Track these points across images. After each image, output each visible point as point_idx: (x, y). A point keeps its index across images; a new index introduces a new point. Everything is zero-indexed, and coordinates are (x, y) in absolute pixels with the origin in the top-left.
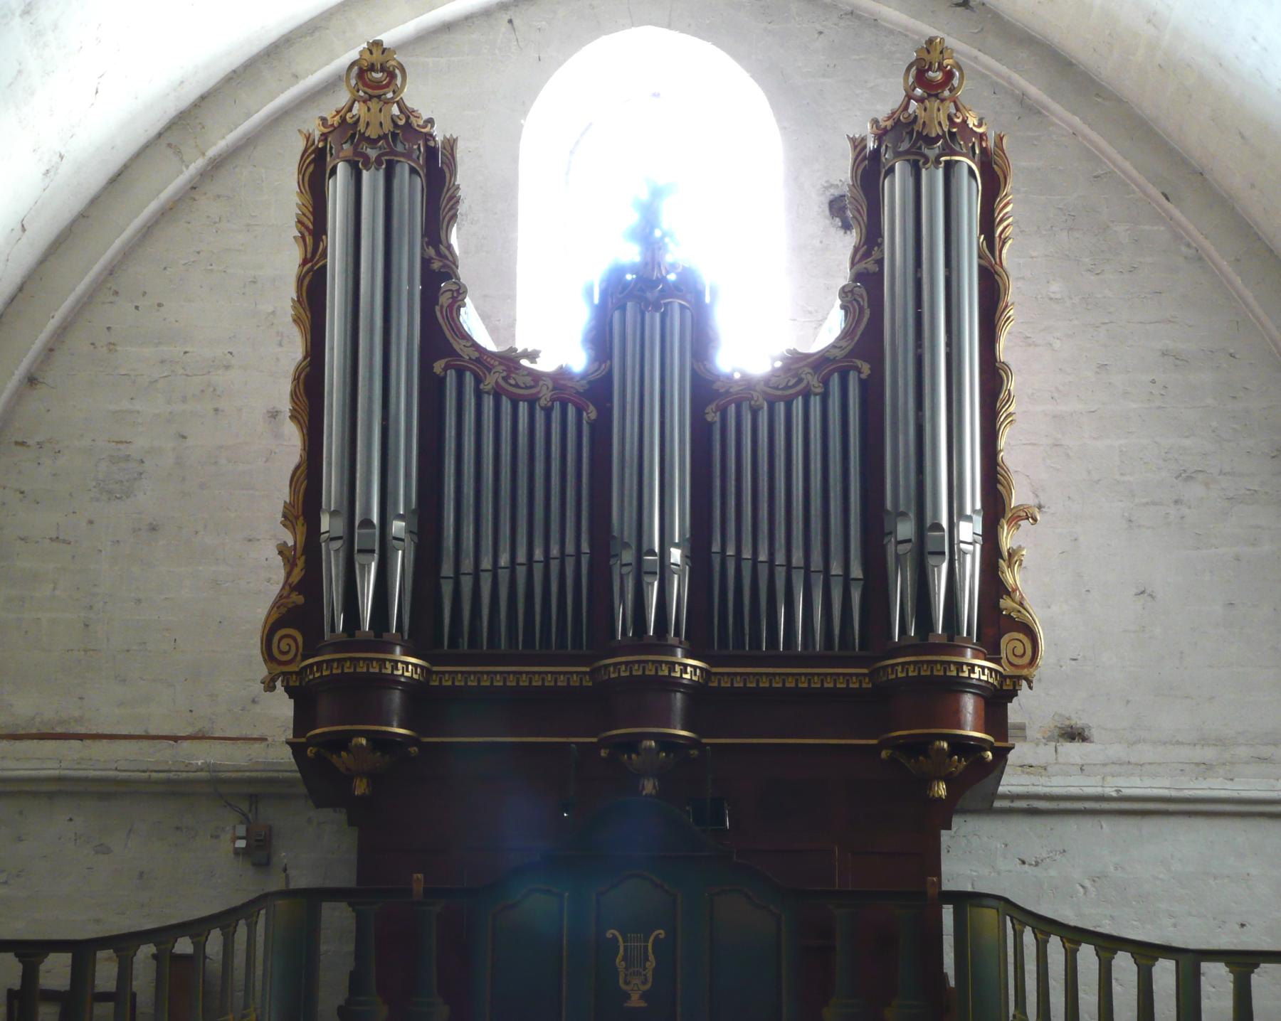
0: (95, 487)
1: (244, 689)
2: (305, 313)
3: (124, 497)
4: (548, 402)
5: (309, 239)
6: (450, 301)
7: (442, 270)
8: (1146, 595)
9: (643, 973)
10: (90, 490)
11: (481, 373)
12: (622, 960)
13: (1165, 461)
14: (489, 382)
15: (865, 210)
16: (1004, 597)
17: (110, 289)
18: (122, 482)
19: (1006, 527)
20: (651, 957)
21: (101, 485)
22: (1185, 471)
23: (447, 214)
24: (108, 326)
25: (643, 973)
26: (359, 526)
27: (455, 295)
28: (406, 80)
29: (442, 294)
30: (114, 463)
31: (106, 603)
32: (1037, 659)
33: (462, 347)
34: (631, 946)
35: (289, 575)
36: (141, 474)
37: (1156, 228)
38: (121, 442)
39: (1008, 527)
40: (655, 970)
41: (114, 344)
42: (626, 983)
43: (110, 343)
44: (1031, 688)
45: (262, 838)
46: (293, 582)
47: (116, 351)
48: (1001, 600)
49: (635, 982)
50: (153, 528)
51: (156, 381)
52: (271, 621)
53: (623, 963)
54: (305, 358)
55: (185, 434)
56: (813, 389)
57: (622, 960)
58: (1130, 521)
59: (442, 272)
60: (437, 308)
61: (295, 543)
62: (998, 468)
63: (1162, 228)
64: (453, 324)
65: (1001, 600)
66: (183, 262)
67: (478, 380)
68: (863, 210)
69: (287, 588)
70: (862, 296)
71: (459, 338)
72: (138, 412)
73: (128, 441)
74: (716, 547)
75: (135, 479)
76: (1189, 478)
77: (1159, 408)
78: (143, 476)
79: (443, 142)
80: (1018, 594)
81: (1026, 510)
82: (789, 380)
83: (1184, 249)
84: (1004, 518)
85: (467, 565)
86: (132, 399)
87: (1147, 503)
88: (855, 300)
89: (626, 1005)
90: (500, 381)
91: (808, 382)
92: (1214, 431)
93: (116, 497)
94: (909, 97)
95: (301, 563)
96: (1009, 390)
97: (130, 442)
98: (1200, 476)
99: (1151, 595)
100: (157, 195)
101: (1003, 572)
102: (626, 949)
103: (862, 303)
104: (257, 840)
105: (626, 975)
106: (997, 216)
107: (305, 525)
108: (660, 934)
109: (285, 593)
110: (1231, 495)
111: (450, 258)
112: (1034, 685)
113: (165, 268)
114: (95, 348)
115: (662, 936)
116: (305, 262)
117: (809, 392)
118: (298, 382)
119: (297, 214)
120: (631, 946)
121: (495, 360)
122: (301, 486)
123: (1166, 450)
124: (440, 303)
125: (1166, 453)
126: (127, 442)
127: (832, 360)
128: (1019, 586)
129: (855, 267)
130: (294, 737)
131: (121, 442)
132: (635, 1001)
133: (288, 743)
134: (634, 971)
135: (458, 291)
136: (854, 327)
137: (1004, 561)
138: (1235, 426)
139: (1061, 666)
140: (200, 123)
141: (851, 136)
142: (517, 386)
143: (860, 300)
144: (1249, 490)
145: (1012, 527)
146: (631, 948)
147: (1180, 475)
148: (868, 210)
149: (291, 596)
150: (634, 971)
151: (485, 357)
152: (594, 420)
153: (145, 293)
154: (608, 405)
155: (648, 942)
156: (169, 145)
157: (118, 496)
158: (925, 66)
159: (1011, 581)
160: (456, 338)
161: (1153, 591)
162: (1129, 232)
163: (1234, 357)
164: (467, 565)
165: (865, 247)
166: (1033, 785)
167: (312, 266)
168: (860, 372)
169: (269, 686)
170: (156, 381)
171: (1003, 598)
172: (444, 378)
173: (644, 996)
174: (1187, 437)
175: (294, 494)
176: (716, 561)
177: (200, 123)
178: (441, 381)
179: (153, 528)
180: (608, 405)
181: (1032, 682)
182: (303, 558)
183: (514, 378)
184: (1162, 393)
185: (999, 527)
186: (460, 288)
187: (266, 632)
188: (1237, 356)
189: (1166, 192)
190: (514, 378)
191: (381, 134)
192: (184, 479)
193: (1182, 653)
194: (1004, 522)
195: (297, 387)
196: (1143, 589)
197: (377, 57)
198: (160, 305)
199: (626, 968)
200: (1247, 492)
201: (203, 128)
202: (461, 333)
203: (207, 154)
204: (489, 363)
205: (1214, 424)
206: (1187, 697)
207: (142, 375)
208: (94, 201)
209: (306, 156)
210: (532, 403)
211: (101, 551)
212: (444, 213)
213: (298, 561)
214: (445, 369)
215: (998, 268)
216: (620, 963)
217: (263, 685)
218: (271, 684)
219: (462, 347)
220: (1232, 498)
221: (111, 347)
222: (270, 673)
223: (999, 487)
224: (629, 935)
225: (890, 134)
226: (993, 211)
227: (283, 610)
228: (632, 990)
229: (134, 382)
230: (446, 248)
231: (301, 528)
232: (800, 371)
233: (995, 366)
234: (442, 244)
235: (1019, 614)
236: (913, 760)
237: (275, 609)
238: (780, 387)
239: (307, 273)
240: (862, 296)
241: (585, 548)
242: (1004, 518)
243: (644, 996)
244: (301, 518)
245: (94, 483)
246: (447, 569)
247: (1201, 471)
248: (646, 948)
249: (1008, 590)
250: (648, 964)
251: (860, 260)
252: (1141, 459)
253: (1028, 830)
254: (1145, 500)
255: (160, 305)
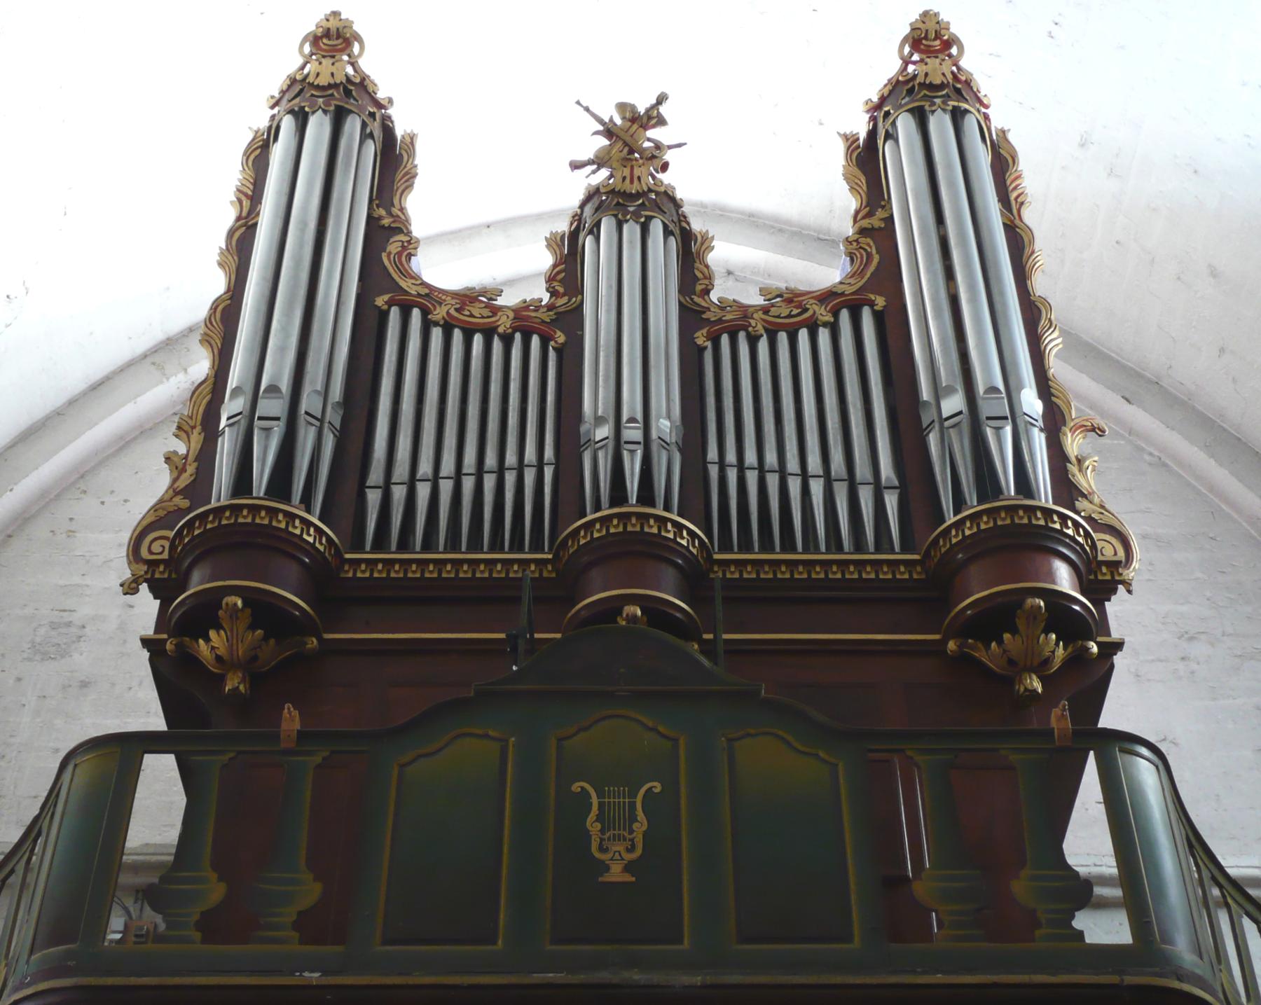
0: (29, 648)
1: (160, 835)
2: (233, 258)
3: (59, 657)
4: (508, 329)
5: (246, 203)
6: (400, 249)
7: (392, 225)
8: (1168, 742)
9: (628, 837)
10: (23, 651)
11: (430, 306)
12: (597, 821)
13: (1163, 624)
14: (439, 313)
15: (864, 182)
16: (1080, 499)
17: (79, 488)
18: (59, 645)
19: (1069, 435)
20: (640, 815)
21: (37, 648)
22: (1186, 633)
23: (401, 184)
24: (71, 517)
25: (628, 837)
26: (263, 392)
27: (406, 244)
28: (364, 46)
29: (391, 244)
30: (54, 629)
31: (20, 752)
32: (1132, 561)
33: (410, 285)
34: (609, 802)
35: (175, 481)
36: (81, 637)
37: (1116, 442)
38: (64, 611)
39: (1072, 435)
40: (645, 834)
41: (74, 532)
42: (602, 849)
43: (70, 531)
44: (1129, 592)
45: (144, 932)
46: (178, 487)
47: (75, 537)
48: (1076, 502)
49: (618, 848)
50: (84, 685)
51: (111, 560)
52: (145, 523)
53: (599, 826)
54: (225, 293)
55: (132, 604)
56: (820, 317)
57: (597, 821)
58: (1138, 676)
59: (393, 228)
60: (384, 256)
61: (188, 451)
62: (1050, 382)
63: (1122, 442)
64: (400, 267)
65: (1076, 502)
66: (155, 468)
67: (425, 312)
68: (861, 181)
69: (171, 492)
70: (868, 245)
71: (406, 277)
72: (88, 586)
73: (72, 609)
74: (712, 454)
75: (74, 642)
76: (1191, 639)
77: (1149, 580)
78: (82, 639)
79: (403, 137)
80: (1096, 497)
81: (1091, 421)
82: (792, 311)
83: (1147, 457)
84: (1065, 426)
85: (401, 470)
86: (83, 575)
87: (1153, 661)
88: (861, 248)
89: (600, 879)
90: (453, 312)
91: (815, 312)
92: (1208, 599)
93: (50, 657)
94: (906, 62)
95: (191, 469)
96: (1050, 319)
97: (74, 611)
98: (1203, 637)
99: (1172, 742)
100: (135, 398)
101: (1073, 476)
102: (601, 805)
103: (869, 250)
104: (136, 936)
105: (602, 840)
106: (1010, 185)
107: (203, 434)
108: (655, 787)
109: (167, 497)
110: (1239, 653)
111: (403, 217)
112: (1134, 587)
113: (137, 472)
114: (54, 534)
115: (657, 790)
116: (239, 219)
117: (816, 322)
118: (215, 312)
119: (237, 186)
120: (614, 802)
121: (447, 296)
122: (204, 398)
123: (1163, 616)
124: (388, 251)
125: (1163, 618)
126: (70, 611)
127: (840, 294)
128: (1094, 487)
129: (856, 225)
130: (156, 632)
131: (64, 611)
132: (616, 873)
133: (146, 642)
134: (614, 835)
135: (409, 242)
136: (863, 269)
137: (1074, 466)
138: (1229, 595)
139: (1087, 809)
140: (186, 348)
141: (842, 133)
142: (472, 316)
143: (867, 248)
144: (1257, 649)
145: (1078, 435)
146: (609, 807)
147: (1182, 636)
148: (867, 183)
149: (174, 499)
150: (614, 835)
151: (436, 294)
152: (562, 344)
153: (112, 492)
154: (579, 333)
155: (635, 797)
156: (154, 364)
157: (52, 656)
158: (921, 34)
159: (1085, 484)
160: (403, 277)
161: (1174, 739)
162: (1091, 445)
163: (1215, 540)
164: (401, 470)
165: (868, 209)
166: (1095, 865)
167: (247, 222)
168: (871, 304)
169: (130, 588)
170: (111, 560)
171: (1078, 501)
172: (387, 313)
173: (628, 868)
174: (1182, 604)
175: (194, 406)
176: (714, 471)
177: (186, 348)
178: (383, 316)
179: (84, 685)
180: (579, 333)
181: (1130, 585)
182: (196, 464)
183: (468, 310)
184: (1150, 568)
185: (1061, 434)
186: (411, 239)
187: (137, 532)
188: (1218, 539)
189: (1127, 396)
190: (468, 310)
191: (332, 82)
192: (125, 642)
193: (1218, 796)
194: (1066, 429)
195: (213, 315)
196: (1163, 737)
197: (333, 24)
198: (126, 501)
199: (602, 831)
200: (1255, 650)
201: (188, 351)
202: (409, 274)
203: (190, 370)
204: (440, 298)
205: (1208, 594)
206: (1233, 838)
207: (97, 556)
208: (72, 402)
209: (250, 151)
210: (489, 333)
211: (24, 705)
212: (399, 184)
213: (188, 467)
214: (390, 303)
215: (1017, 222)
216: (593, 826)
217: (121, 588)
218: (134, 585)
219: (410, 285)
220: (1240, 656)
221: (70, 534)
222: (133, 575)
223: (1054, 399)
224: (607, 788)
225: (889, 100)
226: (1005, 181)
227: (162, 513)
228: (612, 860)
229: (88, 562)
230: (399, 210)
231: (197, 438)
232: (805, 302)
233: (1030, 299)
234: (394, 207)
235: (1101, 516)
236: (994, 644)
237: (152, 511)
238: (782, 315)
239: (241, 226)
240: (868, 245)
241: (549, 453)
242: (1065, 426)
243: (628, 868)
244: (199, 428)
245: (29, 646)
246: (376, 475)
247: (1203, 633)
248: (633, 806)
249: (1084, 494)
250: (635, 826)
251: (863, 218)
252: (1139, 623)
253: (1092, 926)
254: (1151, 658)
255: (126, 501)
